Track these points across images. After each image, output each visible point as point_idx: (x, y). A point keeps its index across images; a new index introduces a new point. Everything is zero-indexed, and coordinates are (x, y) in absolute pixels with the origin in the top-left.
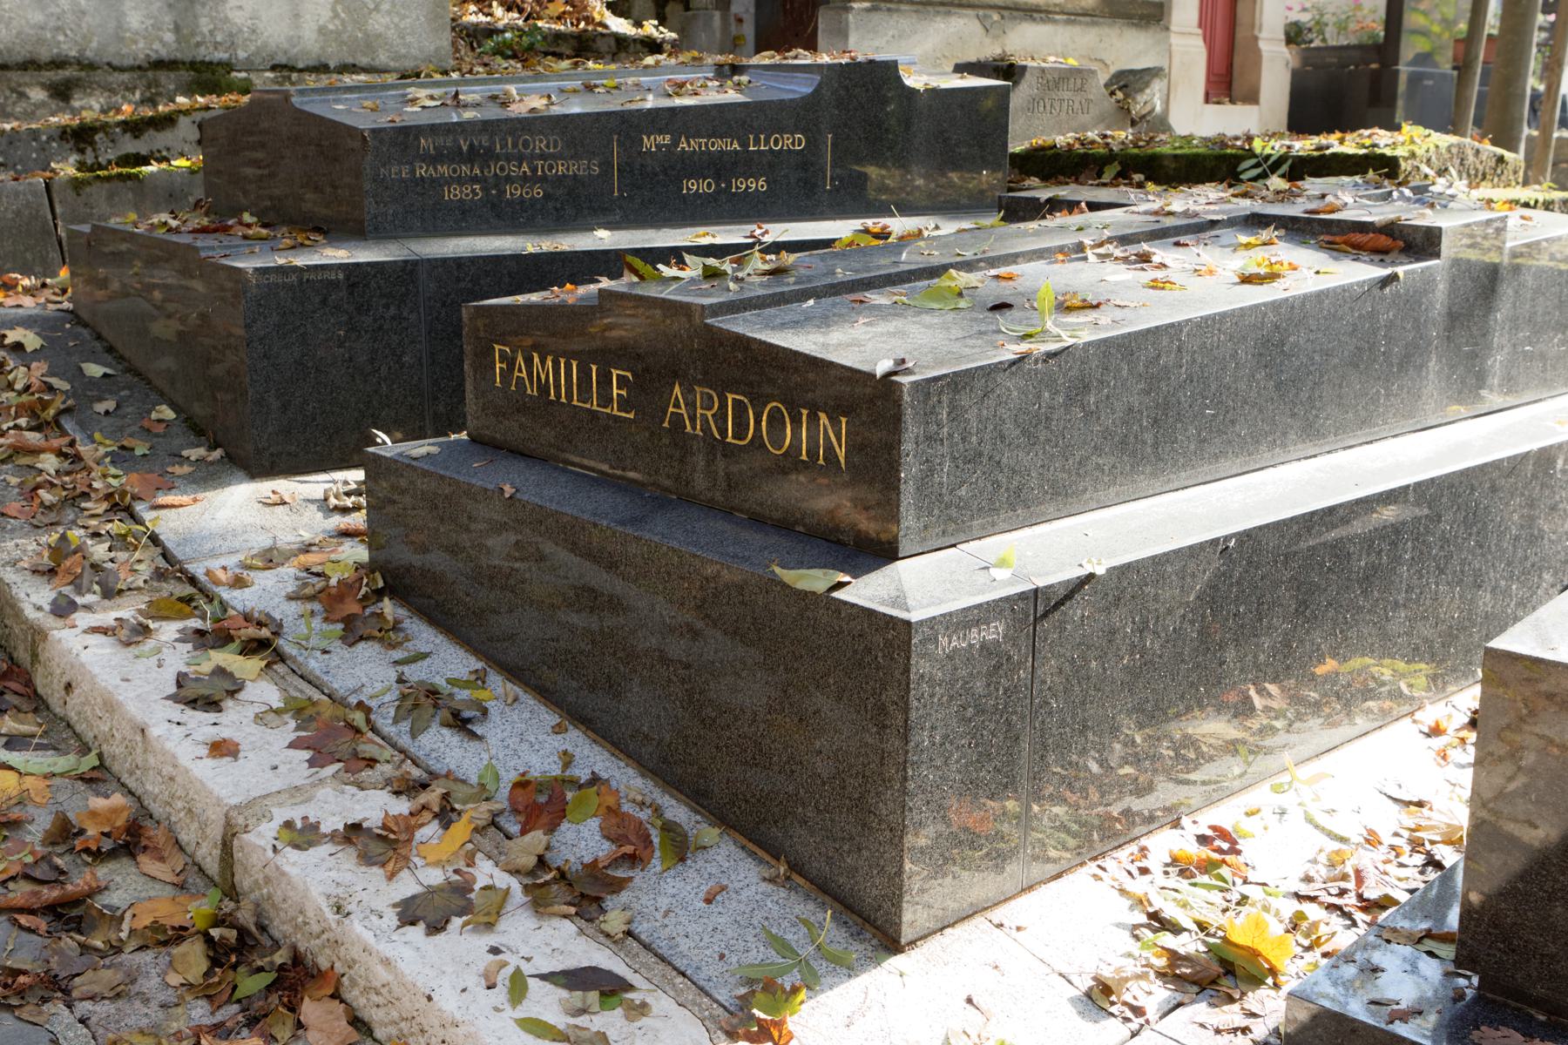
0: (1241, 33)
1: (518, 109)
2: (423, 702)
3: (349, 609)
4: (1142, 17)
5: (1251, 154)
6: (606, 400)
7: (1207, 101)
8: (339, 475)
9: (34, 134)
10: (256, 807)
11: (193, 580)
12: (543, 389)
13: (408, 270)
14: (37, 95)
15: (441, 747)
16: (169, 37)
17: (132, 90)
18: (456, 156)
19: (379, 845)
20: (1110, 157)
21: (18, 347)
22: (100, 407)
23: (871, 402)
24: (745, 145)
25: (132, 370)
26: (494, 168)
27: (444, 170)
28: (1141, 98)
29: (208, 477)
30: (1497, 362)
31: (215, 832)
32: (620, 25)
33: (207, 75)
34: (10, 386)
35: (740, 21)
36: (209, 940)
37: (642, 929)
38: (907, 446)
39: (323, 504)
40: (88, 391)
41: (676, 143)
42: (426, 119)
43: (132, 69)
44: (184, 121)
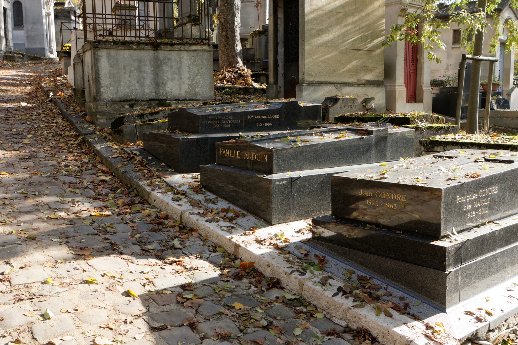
0: (418, 85)
1: (226, 111)
2: (208, 201)
3: (197, 190)
4: (377, 84)
5: (382, 117)
6: (236, 155)
7: (408, 101)
8: (194, 174)
9: (133, 116)
10: (186, 211)
11: (172, 187)
12: (227, 155)
13: (207, 139)
14: (127, 107)
15: (211, 205)
16: (154, 94)
17: (146, 105)
18: (215, 120)
19: (204, 215)
20: (355, 118)
21: (135, 154)
22: (152, 163)
23: (270, 153)
24: (267, 117)
25: (156, 158)
26: (221, 122)
27: (213, 122)
28: (369, 105)
29: (172, 173)
30: (389, 153)
31: (179, 215)
32: (256, 85)
33: (162, 102)
34: (136, 160)
35: (280, 87)
36: (179, 227)
37: (238, 223)
38: (274, 158)
39: (192, 178)
40: (149, 161)
41: (254, 117)
42: (209, 113)
43: (146, 101)
44: (161, 113)
